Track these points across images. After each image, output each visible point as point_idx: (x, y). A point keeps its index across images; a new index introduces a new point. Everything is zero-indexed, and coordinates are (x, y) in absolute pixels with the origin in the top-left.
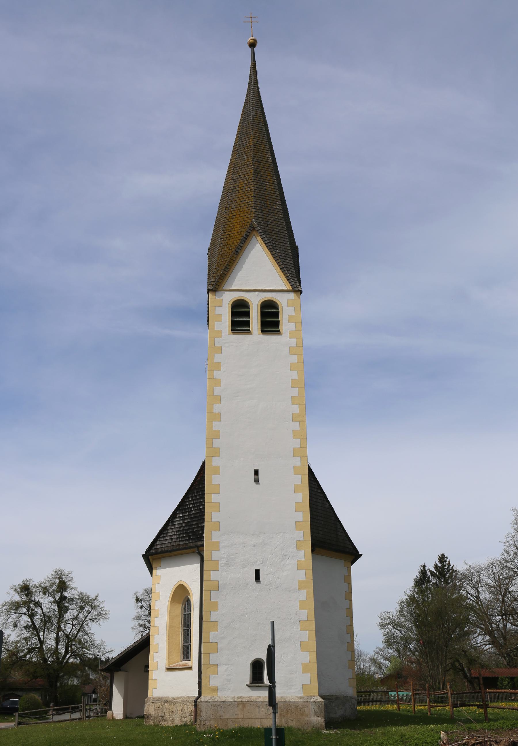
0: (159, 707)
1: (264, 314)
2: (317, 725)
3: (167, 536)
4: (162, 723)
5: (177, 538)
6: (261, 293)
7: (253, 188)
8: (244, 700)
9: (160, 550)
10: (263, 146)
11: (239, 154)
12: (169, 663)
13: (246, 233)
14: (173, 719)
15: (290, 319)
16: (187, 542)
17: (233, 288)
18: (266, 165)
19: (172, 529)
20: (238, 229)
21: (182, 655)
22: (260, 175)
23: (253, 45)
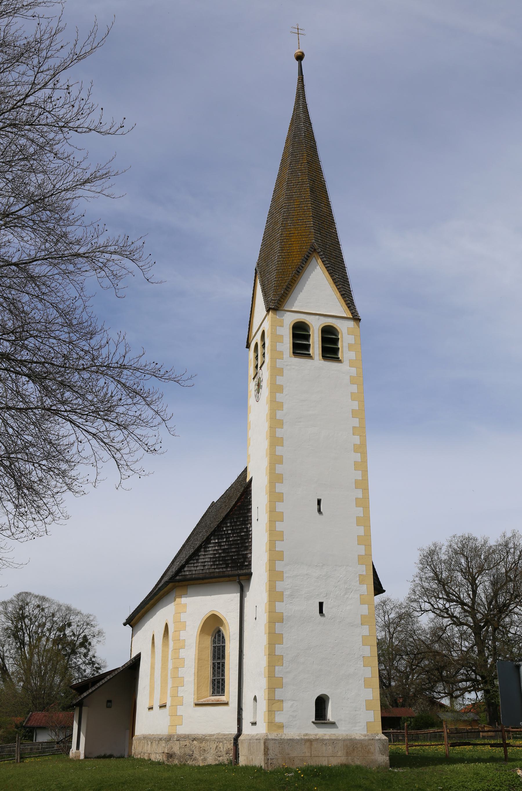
0: (186, 745)
1: (324, 340)
2: (383, 763)
3: (197, 562)
4: (190, 762)
5: (211, 565)
6: (322, 318)
7: (311, 207)
8: (311, 737)
9: (188, 577)
10: (316, 165)
11: (292, 170)
12: (198, 697)
13: (307, 253)
14: (204, 758)
15: (350, 347)
16: (224, 570)
17: (293, 309)
18: (320, 185)
19: (205, 555)
20: (297, 248)
21: (212, 690)
22: (315, 195)
23: (300, 58)
